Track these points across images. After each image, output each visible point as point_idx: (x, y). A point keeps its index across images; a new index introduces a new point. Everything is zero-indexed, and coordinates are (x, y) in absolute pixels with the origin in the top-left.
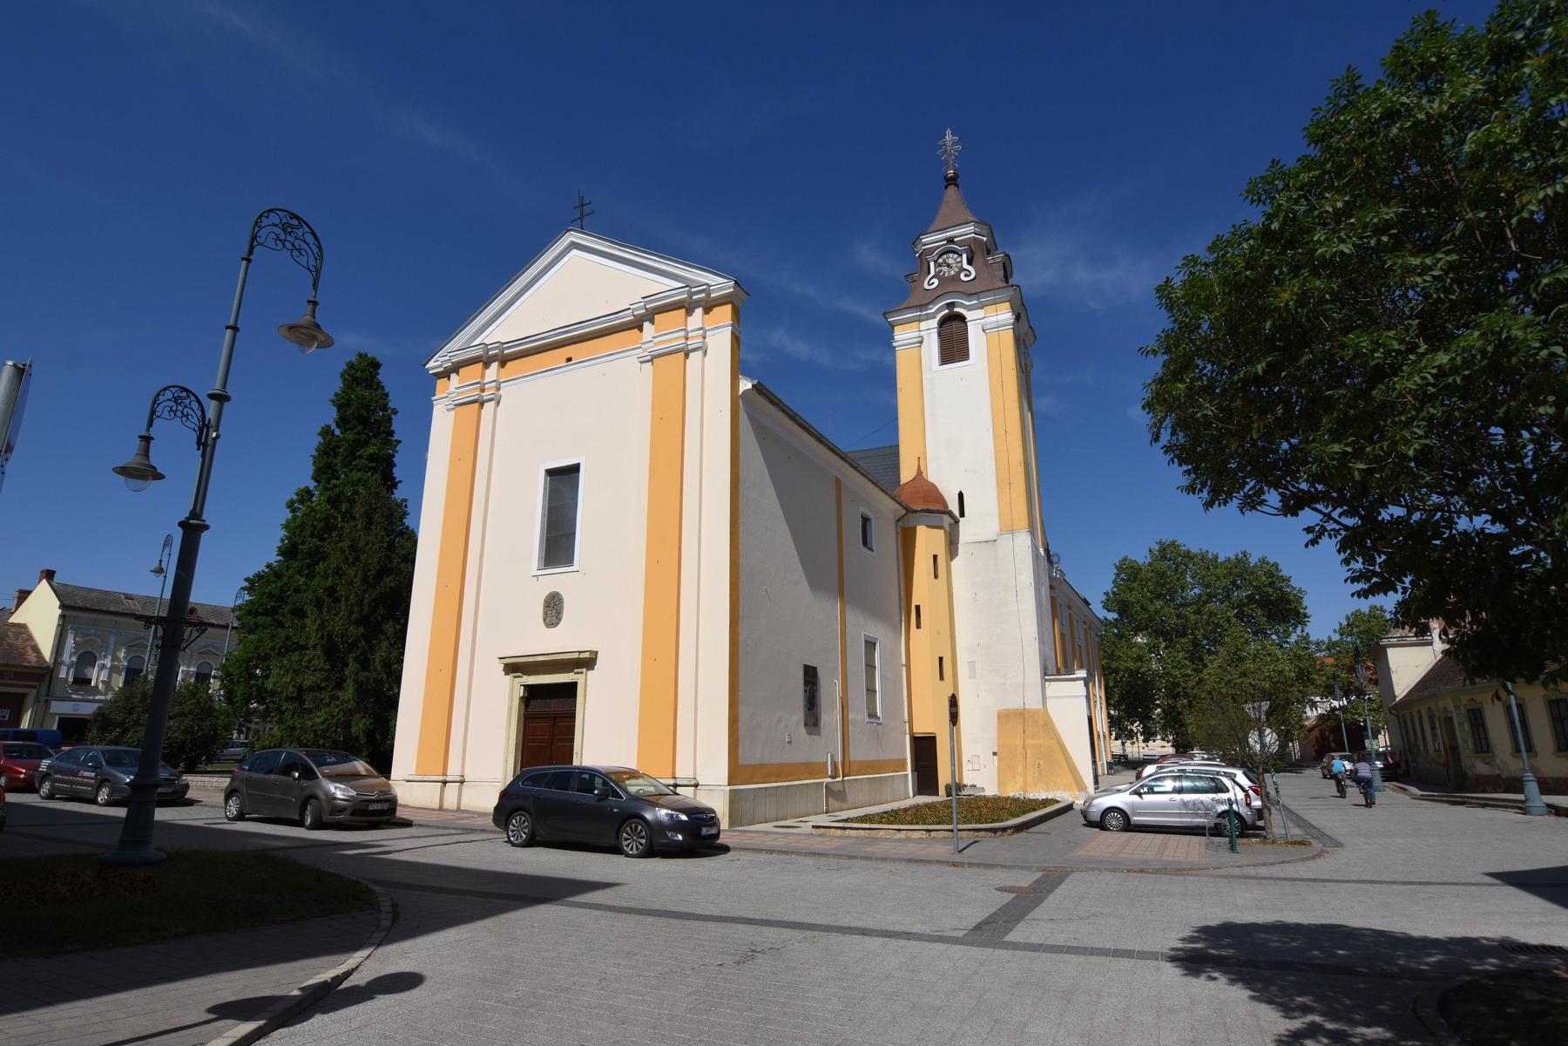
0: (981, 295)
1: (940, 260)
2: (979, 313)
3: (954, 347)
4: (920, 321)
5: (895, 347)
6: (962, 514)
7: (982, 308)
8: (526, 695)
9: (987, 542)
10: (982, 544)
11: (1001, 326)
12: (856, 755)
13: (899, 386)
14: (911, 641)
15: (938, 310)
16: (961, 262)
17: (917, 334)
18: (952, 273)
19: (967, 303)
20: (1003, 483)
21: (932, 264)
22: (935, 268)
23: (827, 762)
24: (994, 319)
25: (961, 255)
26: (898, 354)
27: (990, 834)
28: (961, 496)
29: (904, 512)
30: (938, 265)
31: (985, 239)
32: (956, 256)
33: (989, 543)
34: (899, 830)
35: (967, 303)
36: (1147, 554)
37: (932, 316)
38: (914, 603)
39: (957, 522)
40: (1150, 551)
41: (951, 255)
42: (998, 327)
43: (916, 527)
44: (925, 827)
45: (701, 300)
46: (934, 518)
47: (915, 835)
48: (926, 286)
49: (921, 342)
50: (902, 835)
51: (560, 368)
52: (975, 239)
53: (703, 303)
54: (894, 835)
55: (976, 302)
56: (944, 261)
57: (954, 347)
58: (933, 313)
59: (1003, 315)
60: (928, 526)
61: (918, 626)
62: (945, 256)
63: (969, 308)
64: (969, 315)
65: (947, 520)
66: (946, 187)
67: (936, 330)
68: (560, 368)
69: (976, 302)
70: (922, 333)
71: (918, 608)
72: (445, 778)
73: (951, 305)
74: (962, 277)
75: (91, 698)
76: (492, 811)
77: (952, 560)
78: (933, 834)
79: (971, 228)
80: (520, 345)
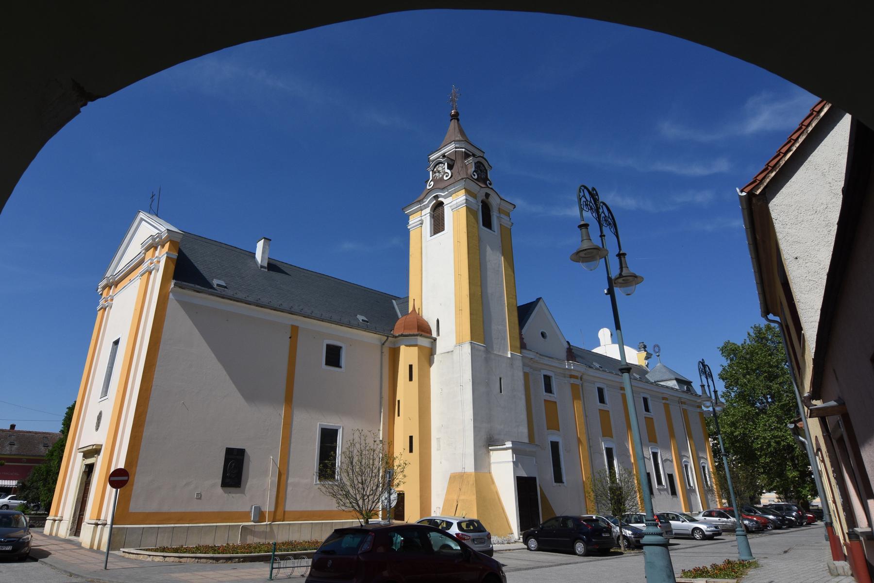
0: (448, 188)
1: (435, 170)
2: (449, 200)
3: (438, 226)
4: (422, 210)
5: (409, 229)
6: (438, 334)
7: (451, 196)
8: (87, 470)
9: (448, 352)
10: (446, 354)
11: (459, 206)
12: (290, 506)
13: (410, 254)
14: (395, 425)
15: (429, 202)
16: (444, 168)
17: (420, 219)
18: (441, 176)
19: (443, 194)
20: (459, 310)
21: (431, 173)
22: (432, 175)
23: (251, 511)
24: (454, 202)
25: (444, 164)
26: (411, 232)
27: (211, 561)
28: (438, 321)
29: (386, 337)
30: (434, 172)
31: (464, 150)
32: (443, 165)
33: (450, 353)
34: (150, 555)
35: (443, 194)
36: (746, 336)
37: (426, 207)
38: (397, 399)
39: (435, 340)
40: (749, 334)
41: (440, 165)
42: (457, 207)
43: (400, 347)
44: (162, 554)
45: (159, 242)
46: (411, 340)
47: (157, 559)
48: (428, 187)
49: (422, 224)
50: (150, 559)
51: (126, 285)
52: (456, 151)
53: (159, 243)
54: (147, 558)
55: (447, 193)
56: (437, 169)
57: (438, 226)
58: (427, 204)
59: (460, 197)
60: (407, 346)
61: (399, 415)
62: (437, 166)
63: (445, 197)
64: (445, 201)
65: (424, 342)
66: (452, 120)
67: (429, 214)
68: (126, 285)
69: (447, 193)
70: (423, 218)
71: (399, 401)
72: (97, 521)
73: (436, 197)
74: (445, 178)
75: (713, 477)
76: (494, 554)
77: (430, 366)
78: (167, 559)
79: (452, 146)
80: (118, 275)
